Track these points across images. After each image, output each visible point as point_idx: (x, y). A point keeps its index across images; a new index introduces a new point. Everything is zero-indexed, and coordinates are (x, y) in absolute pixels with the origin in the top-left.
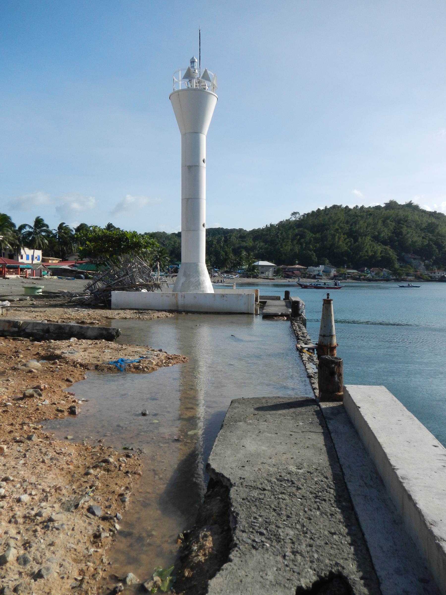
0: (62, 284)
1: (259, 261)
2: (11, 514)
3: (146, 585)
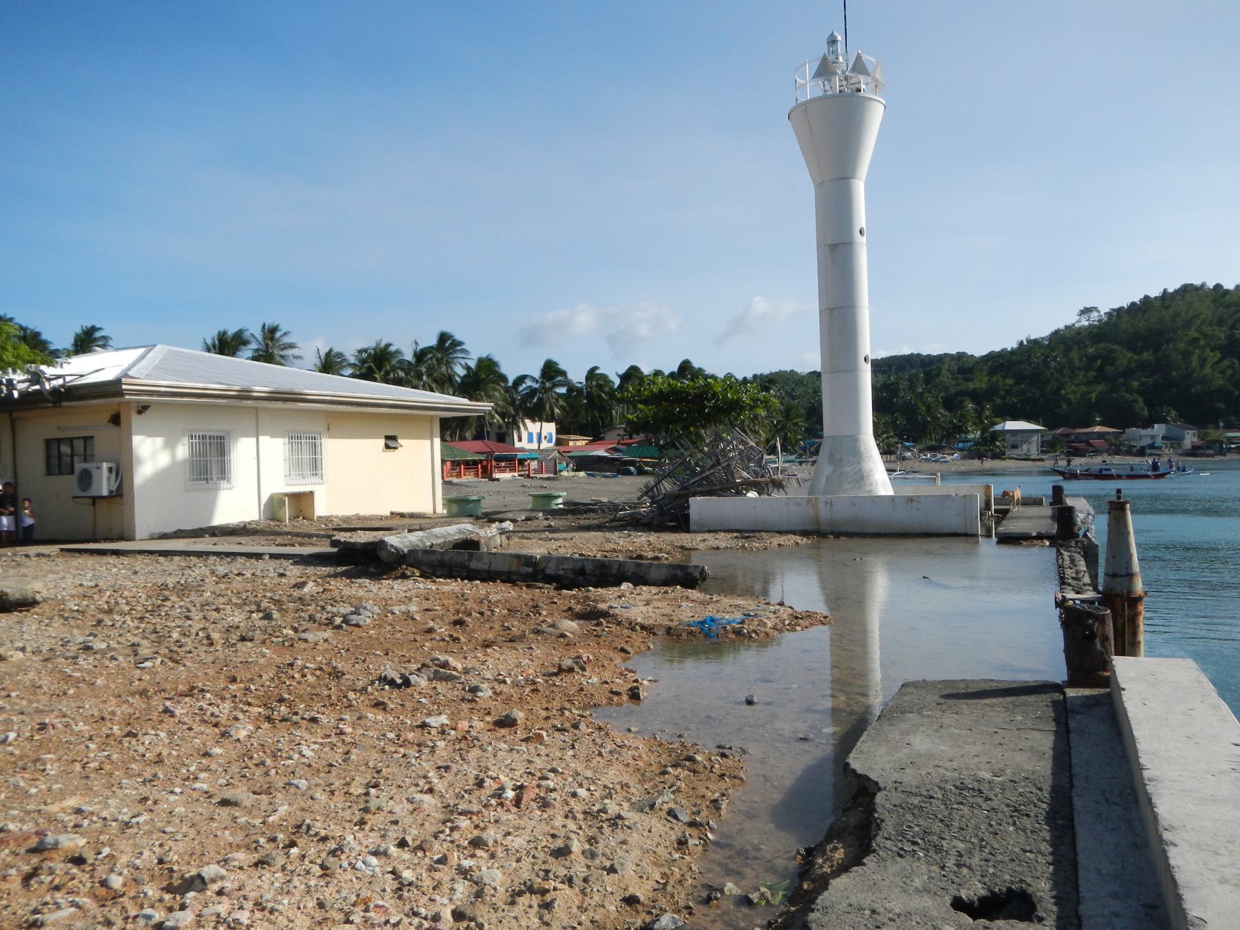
0: (595, 487)
1: (1004, 421)
2: (567, 808)
3: (751, 896)
